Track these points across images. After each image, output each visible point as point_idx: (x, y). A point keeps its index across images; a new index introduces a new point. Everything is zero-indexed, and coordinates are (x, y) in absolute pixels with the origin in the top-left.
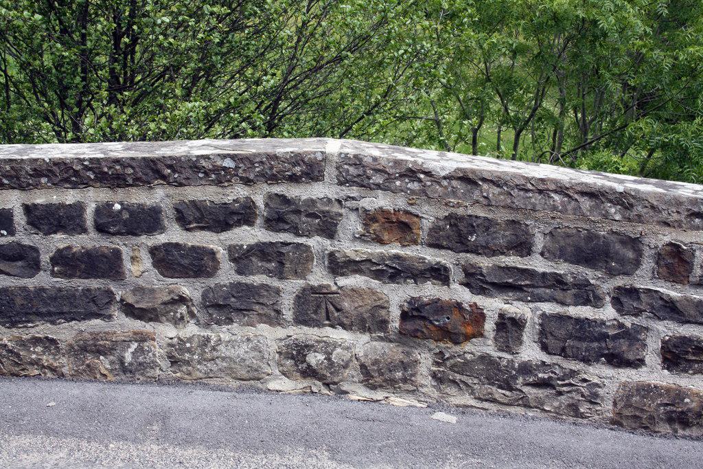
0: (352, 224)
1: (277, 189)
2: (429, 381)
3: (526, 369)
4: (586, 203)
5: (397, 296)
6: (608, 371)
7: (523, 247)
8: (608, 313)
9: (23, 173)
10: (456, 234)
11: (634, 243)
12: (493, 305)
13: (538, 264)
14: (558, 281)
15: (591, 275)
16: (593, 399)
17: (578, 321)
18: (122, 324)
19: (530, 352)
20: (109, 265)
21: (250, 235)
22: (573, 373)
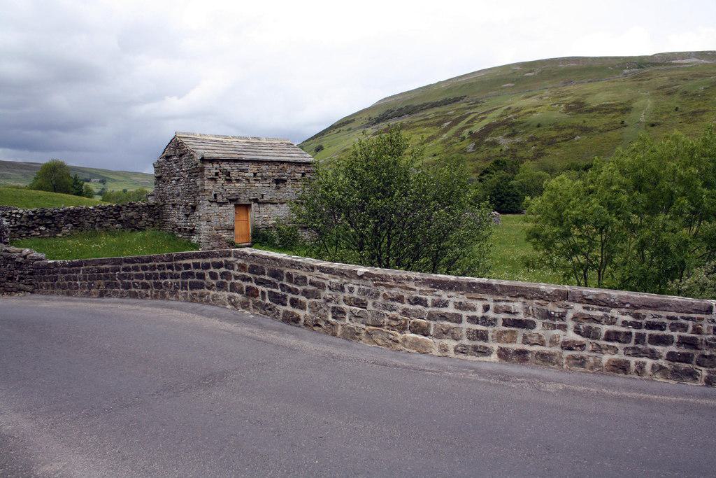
0: (451, 305)
1: (144, 264)
2: (252, 307)
3: (267, 305)
4: (273, 262)
5: (245, 284)
6: (281, 307)
7: (263, 273)
8: (279, 291)
9: (69, 186)
10: (253, 270)
11: (282, 272)
12: (260, 288)
13: (267, 278)
14: (269, 282)
15: (276, 280)
16: (278, 314)
17: (274, 293)
18: (206, 290)
19: (268, 301)
20: (201, 276)
21: (223, 269)
22: (274, 307)
